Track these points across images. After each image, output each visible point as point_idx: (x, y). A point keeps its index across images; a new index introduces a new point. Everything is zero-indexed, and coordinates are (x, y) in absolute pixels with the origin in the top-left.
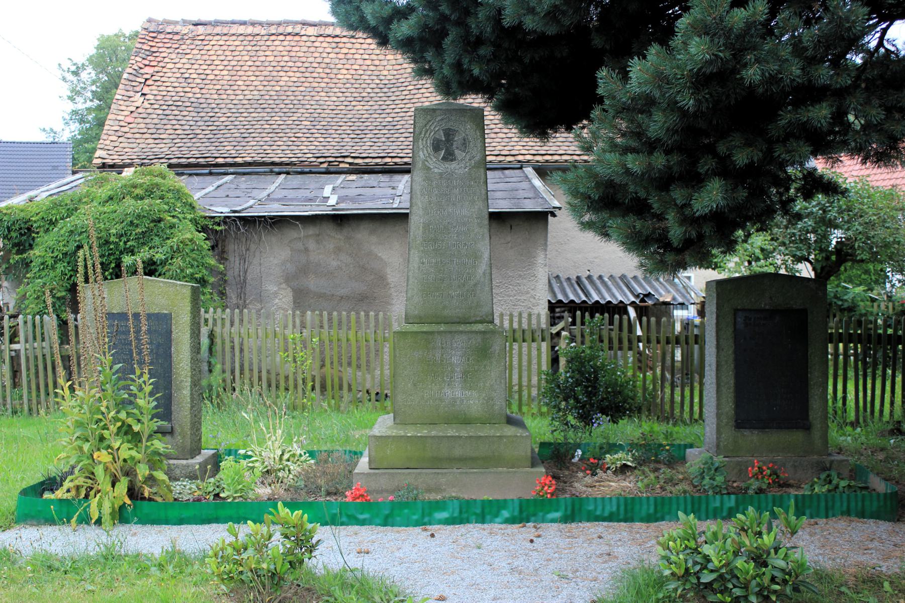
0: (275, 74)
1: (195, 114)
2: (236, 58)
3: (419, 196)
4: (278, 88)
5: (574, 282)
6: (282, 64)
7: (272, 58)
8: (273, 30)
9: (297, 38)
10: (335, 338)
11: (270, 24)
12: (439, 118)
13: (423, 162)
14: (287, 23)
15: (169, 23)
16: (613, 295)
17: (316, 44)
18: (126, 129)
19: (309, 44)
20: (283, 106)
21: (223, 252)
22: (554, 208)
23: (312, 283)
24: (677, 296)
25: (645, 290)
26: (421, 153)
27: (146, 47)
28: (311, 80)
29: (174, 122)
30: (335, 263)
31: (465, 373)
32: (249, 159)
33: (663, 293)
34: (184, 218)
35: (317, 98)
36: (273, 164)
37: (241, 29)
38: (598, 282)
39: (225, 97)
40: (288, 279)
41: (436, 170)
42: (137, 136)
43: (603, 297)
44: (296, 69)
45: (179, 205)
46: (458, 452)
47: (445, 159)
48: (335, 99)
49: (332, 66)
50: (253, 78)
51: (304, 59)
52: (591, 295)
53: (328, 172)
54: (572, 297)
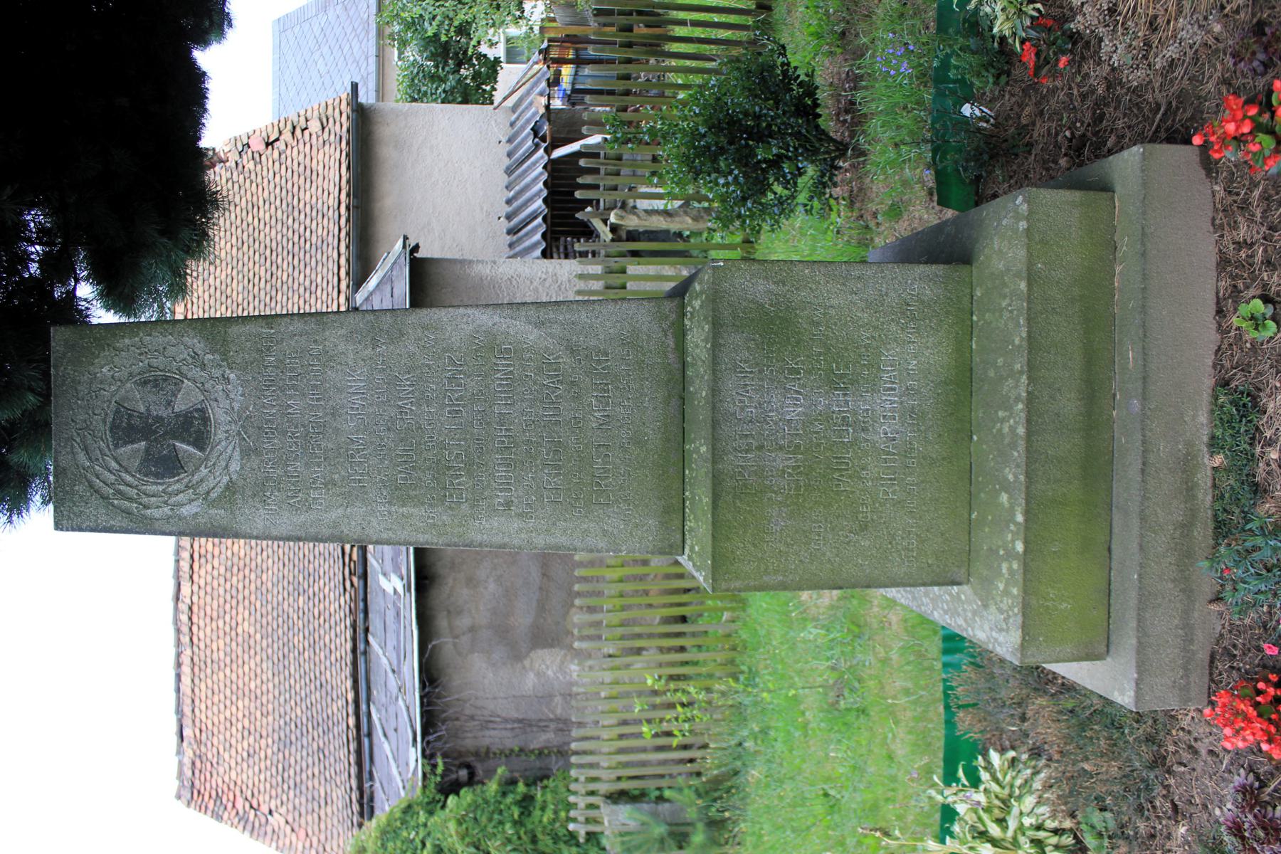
0: (240, 639)
1: (293, 748)
2: (222, 688)
3: (312, 516)
4: (258, 636)
5: (515, 238)
6: (227, 629)
7: (221, 642)
8: (185, 639)
9: (195, 609)
10: (618, 602)
11: (179, 643)
12: (82, 457)
13: (212, 504)
14: (176, 620)
15: (180, 773)
16: (535, 180)
17: (202, 584)
18: (315, 840)
19: (202, 593)
20: (280, 631)
21: (476, 754)
22: (404, 247)
23: (523, 619)
24: (538, 90)
25: (528, 135)
26: (185, 511)
27: (211, 805)
28: (247, 592)
29: (304, 776)
30: (492, 586)
31: (834, 382)
32: (349, 683)
33: (533, 109)
34: (425, 825)
35: (270, 585)
36: (354, 650)
37: (186, 680)
38: (515, 204)
39: (270, 707)
40: (517, 656)
41: (235, 466)
42: (323, 826)
43: (538, 194)
44: (234, 612)
45: (405, 834)
46: (1069, 404)
47: (200, 441)
48: (270, 561)
49: (229, 563)
50: (246, 668)
51: (222, 600)
52: (535, 211)
53: (364, 576)
54: (538, 236)
